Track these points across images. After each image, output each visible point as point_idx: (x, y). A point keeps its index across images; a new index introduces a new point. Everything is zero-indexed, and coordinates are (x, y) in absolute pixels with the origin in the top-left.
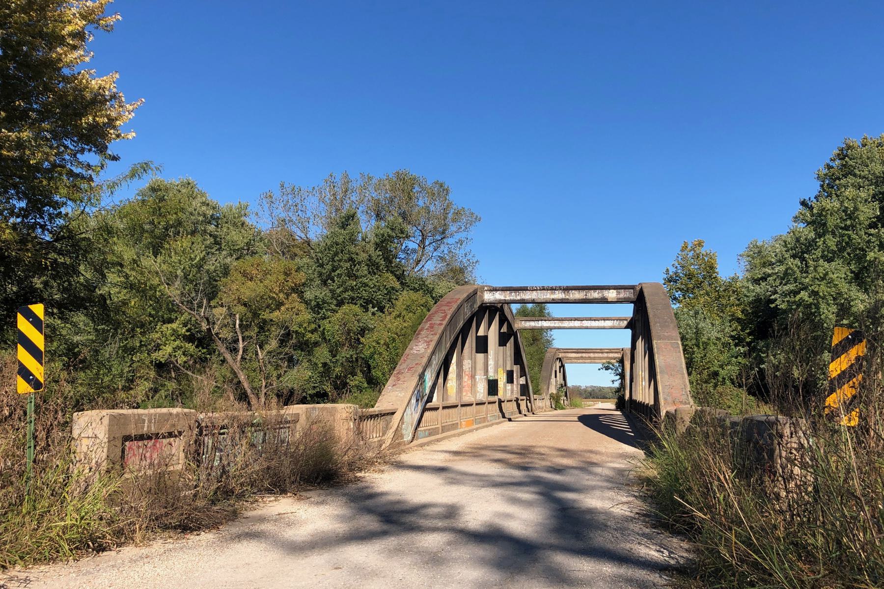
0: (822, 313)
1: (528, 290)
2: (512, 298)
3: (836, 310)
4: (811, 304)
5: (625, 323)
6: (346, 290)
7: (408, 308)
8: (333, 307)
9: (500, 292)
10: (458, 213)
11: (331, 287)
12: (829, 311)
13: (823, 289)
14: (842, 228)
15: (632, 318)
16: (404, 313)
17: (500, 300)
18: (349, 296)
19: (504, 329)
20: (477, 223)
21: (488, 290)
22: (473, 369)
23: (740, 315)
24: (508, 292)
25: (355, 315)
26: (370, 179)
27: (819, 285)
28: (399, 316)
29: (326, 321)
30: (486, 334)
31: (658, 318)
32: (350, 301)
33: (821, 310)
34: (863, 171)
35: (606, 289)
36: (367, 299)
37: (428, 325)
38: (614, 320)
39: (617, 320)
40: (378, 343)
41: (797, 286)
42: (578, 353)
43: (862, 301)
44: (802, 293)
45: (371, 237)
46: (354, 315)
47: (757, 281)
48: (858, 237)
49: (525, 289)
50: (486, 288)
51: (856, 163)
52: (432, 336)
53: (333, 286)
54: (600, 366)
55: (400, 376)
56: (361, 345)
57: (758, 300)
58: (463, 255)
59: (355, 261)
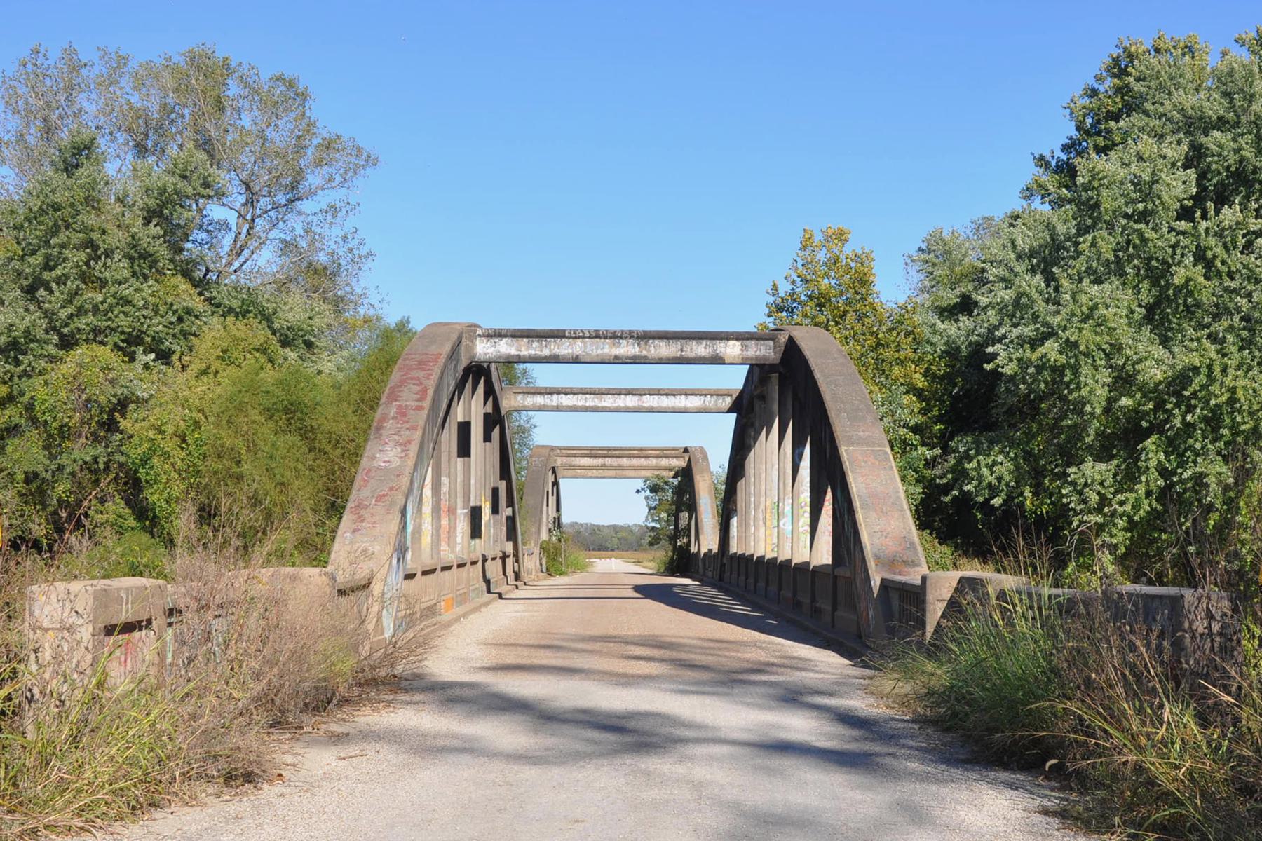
0: (1083, 384)
1: (564, 337)
2: (533, 352)
3: (1110, 380)
4: (1063, 366)
5: (728, 401)
6: (81, 311)
7: (225, 356)
8: (52, 349)
9: (509, 340)
10: (328, 145)
11: (47, 305)
12: (1097, 382)
13: (1087, 337)
14: (1126, 216)
15: (742, 392)
16: (217, 365)
17: (509, 356)
18: (88, 325)
19: (489, 409)
20: (369, 171)
21: (484, 336)
22: (453, 496)
23: (920, 381)
24: (525, 340)
25: (106, 369)
26: (123, 60)
27: (1080, 330)
28: (204, 372)
29: (37, 382)
30: (467, 420)
31: (842, 402)
32: (91, 336)
33: (1082, 379)
34: (1162, 104)
35: (722, 339)
36: (129, 334)
37: (393, 411)
38: (705, 395)
39: (712, 395)
40: (160, 431)
41: (1037, 329)
42: (595, 456)
43: (1159, 362)
44: (1048, 344)
45: (134, 191)
46: (102, 370)
47: (949, 312)
48: (1158, 239)
49: (558, 335)
50: (479, 332)
51: (1149, 87)
52: (407, 433)
53: (50, 302)
54: (639, 484)
55: (362, 512)
56: (120, 436)
57: (951, 352)
58: (339, 240)
59: (98, 248)
